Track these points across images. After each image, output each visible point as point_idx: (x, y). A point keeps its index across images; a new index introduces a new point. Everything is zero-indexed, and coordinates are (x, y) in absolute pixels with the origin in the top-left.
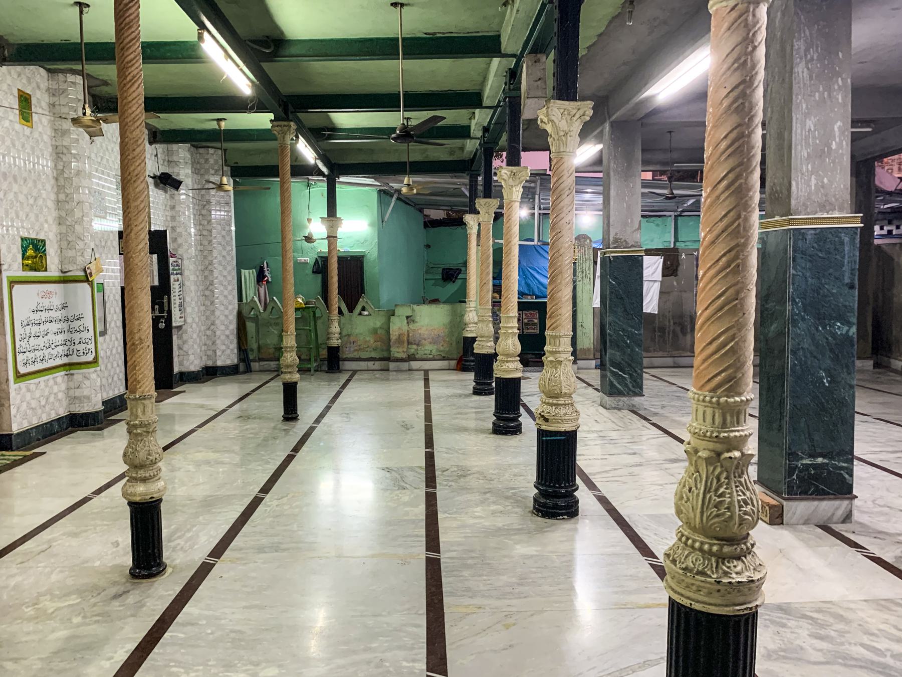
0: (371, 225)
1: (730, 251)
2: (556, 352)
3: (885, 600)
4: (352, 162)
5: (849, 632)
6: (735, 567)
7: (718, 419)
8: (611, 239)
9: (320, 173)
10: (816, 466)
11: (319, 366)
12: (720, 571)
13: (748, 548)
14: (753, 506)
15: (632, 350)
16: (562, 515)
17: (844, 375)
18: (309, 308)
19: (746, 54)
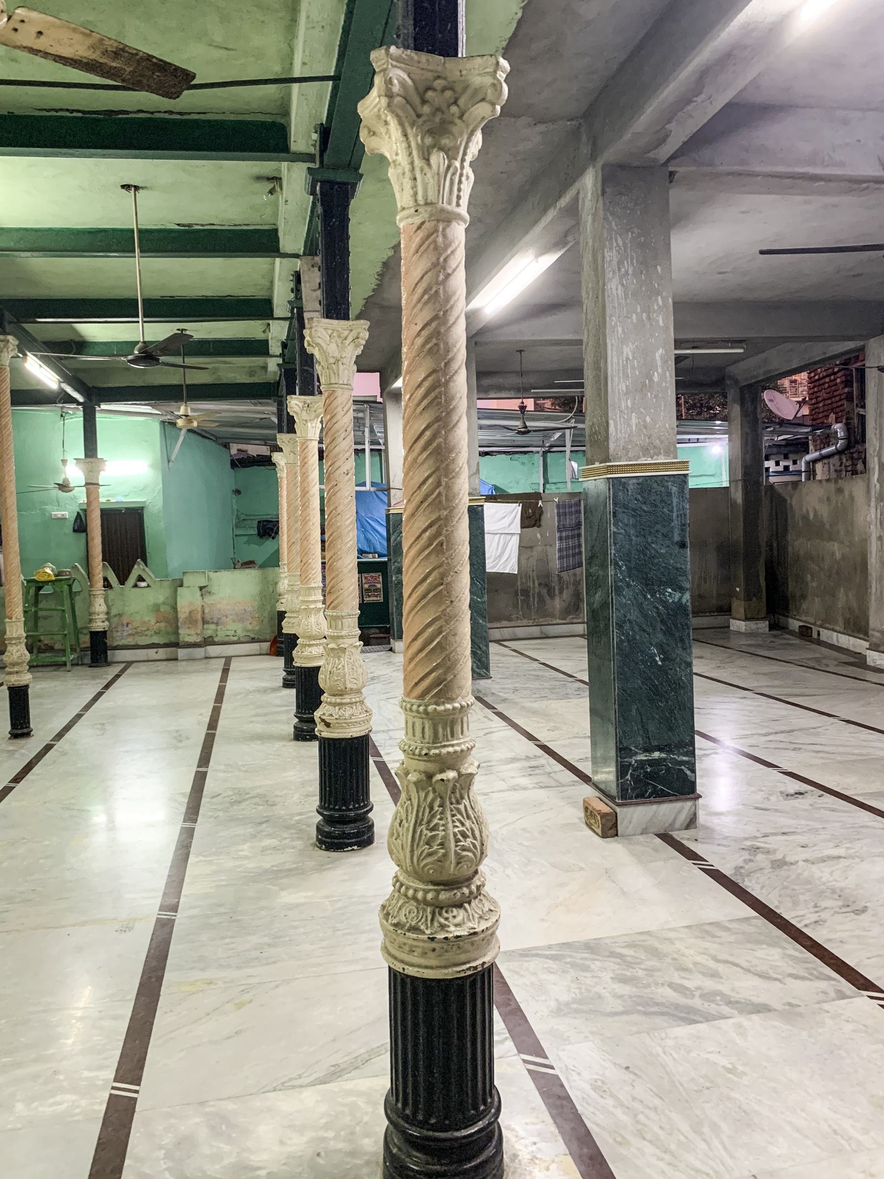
0: (153, 466)
1: (430, 526)
2: (339, 637)
3: (711, 924)
4: (116, 385)
5: (659, 970)
6: (454, 917)
9: (73, 401)
10: (651, 763)
11: (81, 658)
12: (436, 924)
13: (471, 893)
14: (475, 838)
16: (351, 845)
17: (679, 651)
18: (61, 580)
19: (437, 284)
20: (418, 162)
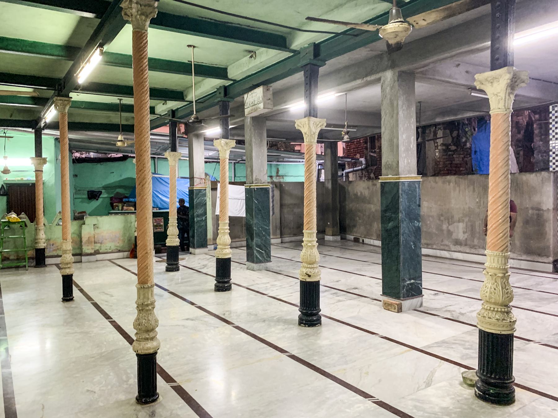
7: (503, 262)
8: (254, 179)
10: (411, 284)
15: (266, 238)
20: (507, 97)
